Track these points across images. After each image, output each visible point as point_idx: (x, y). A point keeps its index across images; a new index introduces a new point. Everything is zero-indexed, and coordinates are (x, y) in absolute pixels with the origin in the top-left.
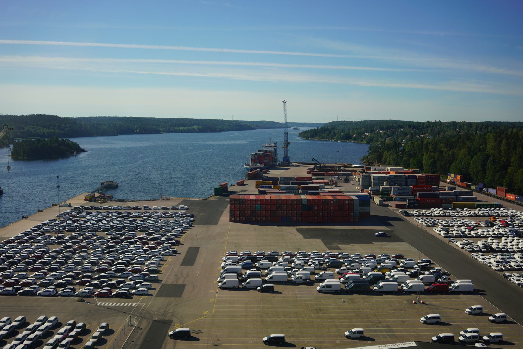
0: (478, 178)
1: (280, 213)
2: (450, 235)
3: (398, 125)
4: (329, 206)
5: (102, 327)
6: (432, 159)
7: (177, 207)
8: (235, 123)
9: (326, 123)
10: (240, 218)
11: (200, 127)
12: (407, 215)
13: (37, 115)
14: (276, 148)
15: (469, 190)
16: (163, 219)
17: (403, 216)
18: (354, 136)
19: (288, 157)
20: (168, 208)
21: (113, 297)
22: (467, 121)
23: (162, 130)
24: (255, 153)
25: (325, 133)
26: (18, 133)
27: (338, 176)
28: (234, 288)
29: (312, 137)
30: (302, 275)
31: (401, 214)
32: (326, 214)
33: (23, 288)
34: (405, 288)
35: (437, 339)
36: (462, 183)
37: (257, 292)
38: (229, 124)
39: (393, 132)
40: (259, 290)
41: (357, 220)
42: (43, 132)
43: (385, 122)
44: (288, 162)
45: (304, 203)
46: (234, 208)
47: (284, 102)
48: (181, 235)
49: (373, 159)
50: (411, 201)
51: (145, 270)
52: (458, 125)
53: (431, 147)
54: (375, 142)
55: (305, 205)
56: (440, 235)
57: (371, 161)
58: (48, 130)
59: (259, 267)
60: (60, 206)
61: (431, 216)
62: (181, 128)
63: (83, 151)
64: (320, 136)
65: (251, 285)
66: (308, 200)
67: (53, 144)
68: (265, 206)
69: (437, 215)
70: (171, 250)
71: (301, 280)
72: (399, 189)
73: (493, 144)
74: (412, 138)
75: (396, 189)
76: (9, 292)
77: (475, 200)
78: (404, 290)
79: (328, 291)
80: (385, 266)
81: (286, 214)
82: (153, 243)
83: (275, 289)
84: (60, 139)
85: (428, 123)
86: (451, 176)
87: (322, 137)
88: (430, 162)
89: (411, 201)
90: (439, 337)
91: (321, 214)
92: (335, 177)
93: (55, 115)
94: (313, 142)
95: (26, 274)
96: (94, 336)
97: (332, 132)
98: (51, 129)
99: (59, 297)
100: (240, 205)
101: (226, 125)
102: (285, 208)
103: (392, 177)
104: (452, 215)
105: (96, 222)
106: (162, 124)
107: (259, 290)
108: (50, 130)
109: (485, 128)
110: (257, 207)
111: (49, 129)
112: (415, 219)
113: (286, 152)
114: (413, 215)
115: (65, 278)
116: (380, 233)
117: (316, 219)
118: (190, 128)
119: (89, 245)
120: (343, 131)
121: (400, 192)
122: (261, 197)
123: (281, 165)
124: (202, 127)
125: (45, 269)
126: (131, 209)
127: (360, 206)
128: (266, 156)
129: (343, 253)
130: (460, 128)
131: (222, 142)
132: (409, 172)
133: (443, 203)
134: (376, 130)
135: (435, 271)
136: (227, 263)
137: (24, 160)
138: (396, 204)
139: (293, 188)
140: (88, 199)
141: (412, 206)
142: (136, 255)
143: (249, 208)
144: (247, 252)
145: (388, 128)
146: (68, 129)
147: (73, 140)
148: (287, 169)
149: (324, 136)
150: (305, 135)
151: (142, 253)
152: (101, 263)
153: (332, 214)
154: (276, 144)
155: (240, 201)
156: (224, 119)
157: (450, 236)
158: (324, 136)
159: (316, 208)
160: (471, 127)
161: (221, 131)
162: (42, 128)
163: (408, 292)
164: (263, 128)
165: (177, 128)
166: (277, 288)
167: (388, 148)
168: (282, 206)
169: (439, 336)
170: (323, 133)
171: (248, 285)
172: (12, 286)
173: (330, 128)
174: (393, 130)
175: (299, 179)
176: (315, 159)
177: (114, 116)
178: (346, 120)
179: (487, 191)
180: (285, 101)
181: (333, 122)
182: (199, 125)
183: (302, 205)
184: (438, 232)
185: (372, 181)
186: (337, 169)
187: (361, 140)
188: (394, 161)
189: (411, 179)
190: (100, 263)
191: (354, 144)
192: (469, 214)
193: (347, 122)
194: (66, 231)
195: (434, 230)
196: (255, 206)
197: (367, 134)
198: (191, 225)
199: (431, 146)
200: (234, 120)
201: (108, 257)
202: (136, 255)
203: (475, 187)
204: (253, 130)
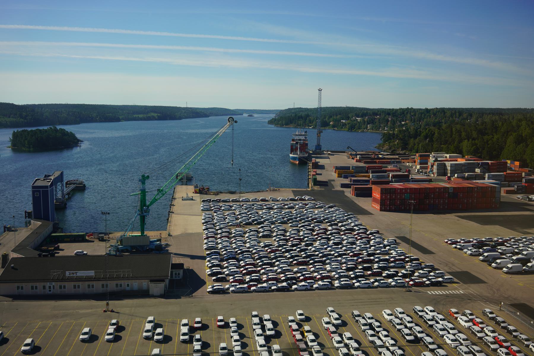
1: (427, 202)
3: (373, 112)
4: (473, 193)
5: (113, 324)
6: (475, 147)
9: (281, 110)
10: (390, 207)
11: (159, 114)
20: (267, 199)
21: (273, 291)
24: (379, 144)
29: (287, 124)
31: (521, 199)
32: (470, 201)
38: (184, 111)
42: (5, 121)
45: (450, 191)
46: (385, 198)
54: (357, 129)
55: (451, 193)
59: (503, 253)
60: (182, 200)
62: (141, 116)
64: (295, 124)
66: (454, 187)
68: (414, 195)
75: (490, 176)
76: (243, 289)
91: (465, 201)
94: (288, 129)
98: (12, 117)
100: (390, 194)
101: (182, 112)
102: (432, 196)
110: (407, 196)
111: (9, 117)
113: (319, 140)
119: (232, 240)
126: (258, 201)
130: (435, 115)
134: (352, 117)
137: (30, 152)
138: (507, 190)
141: (520, 191)
142: (223, 250)
143: (399, 197)
144: (254, 243)
147: (68, 128)
149: (300, 123)
150: (279, 123)
153: (475, 201)
156: (178, 106)
158: (300, 123)
159: (461, 195)
161: (180, 118)
163: (528, 272)
165: (137, 116)
170: (298, 120)
175: (370, 168)
176: (350, 147)
181: (289, 109)
182: (155, 112)
187: (340, 127)
193: (302, 108)
197: (344, 121)
202: (223, 250)
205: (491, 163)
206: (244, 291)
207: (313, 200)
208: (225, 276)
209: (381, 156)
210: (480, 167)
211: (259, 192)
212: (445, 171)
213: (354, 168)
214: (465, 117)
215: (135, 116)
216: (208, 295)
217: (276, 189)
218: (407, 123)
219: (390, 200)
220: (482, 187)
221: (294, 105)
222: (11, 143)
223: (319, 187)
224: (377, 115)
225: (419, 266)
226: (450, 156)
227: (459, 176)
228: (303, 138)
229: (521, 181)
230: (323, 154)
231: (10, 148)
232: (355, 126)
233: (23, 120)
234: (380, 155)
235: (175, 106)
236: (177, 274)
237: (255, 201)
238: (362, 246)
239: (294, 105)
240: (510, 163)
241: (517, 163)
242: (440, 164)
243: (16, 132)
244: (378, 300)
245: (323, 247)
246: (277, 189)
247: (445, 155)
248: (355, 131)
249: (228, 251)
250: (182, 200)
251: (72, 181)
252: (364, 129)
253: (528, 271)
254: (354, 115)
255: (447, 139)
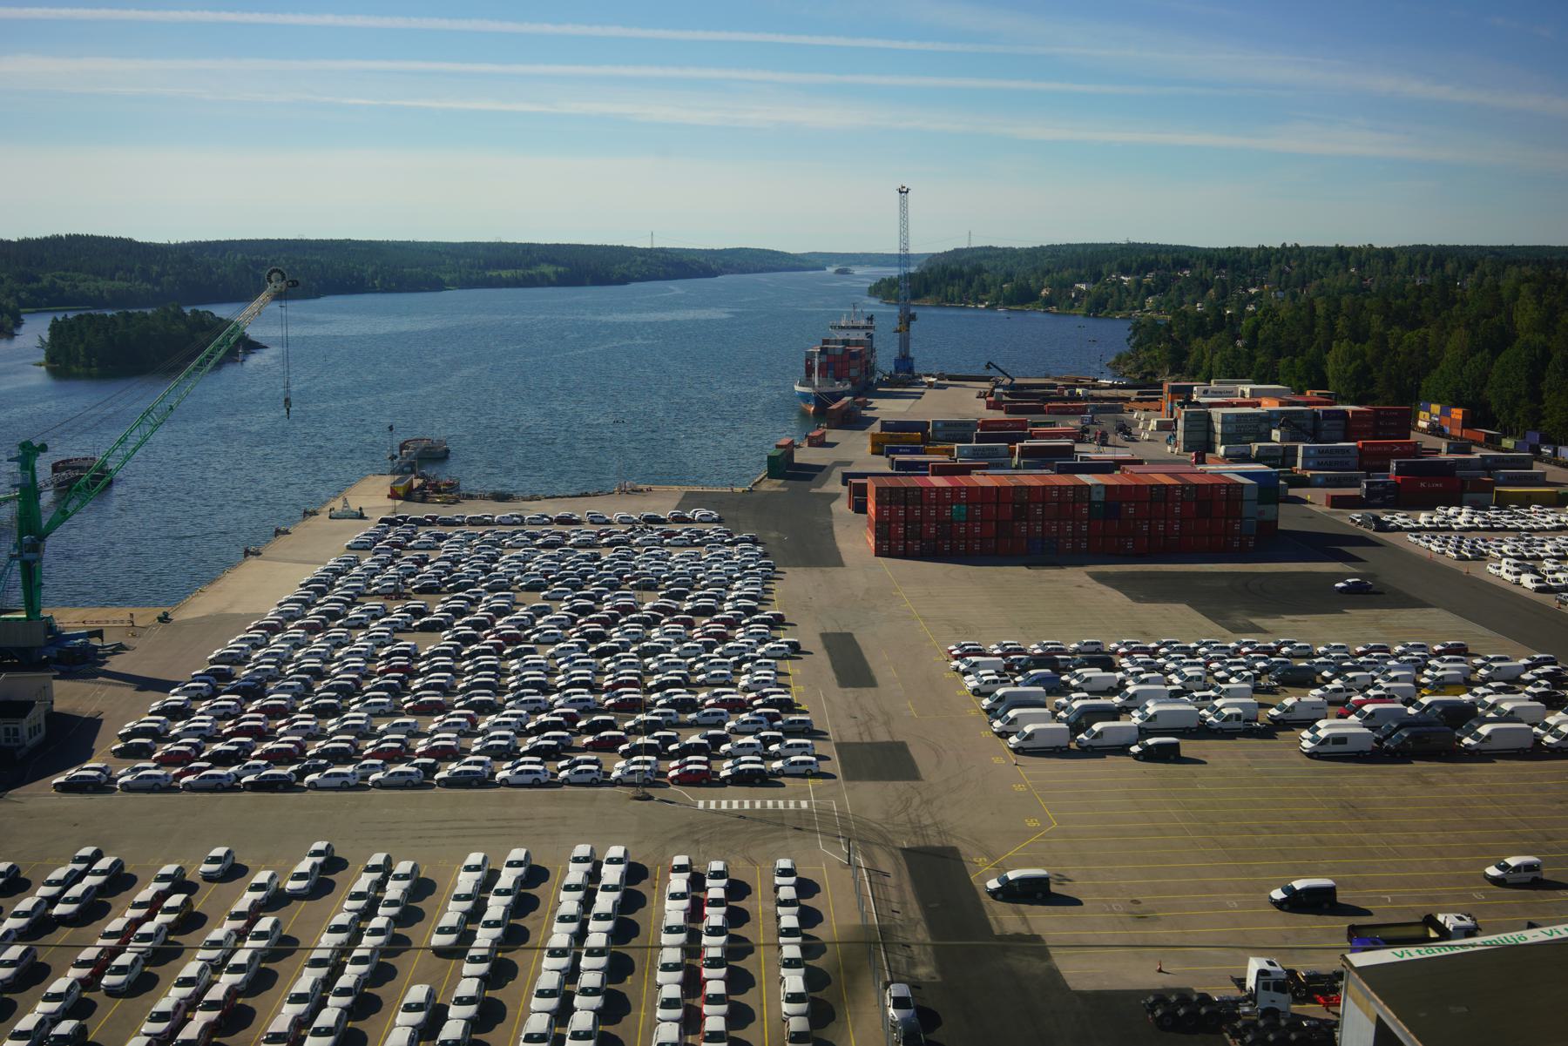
0: (1517, 415)
1: (1024, 529)
2: (1552, 584)
3: (1173, 259)
4: (1077, 505)
7: (689, 515)
8: (661, 255)
9: (934, 255)
10: (905, 545)
11: (560, 269)
12: (1382, 527)
13: (69, 237)
14: (871, 332)
15: (1498, 450)
16: (408, 555)
17: (1371, 532)
18: (1044, 292)
19: (912, 359)
21: (723, 782)
22: (1378, 245)
23: (447, 278)
25: (953, 285)
26: (23, 295)
27: (1091, 413)
28: (1058, 750)
30: (1238, 710)
31: (1359, 523)
32: (1161, 528)
33: (388, 766)
34: (1549, 739)
35: (1284, 896)
36: (1470, 431)
37: (1131, 760)
38: (643, 258)
39: (1162, 280)
40: (1136, 756)
41: (1251, 544)
42: (98, 288)
43: (1131, 248)
44: (910, 376)
45: (1095, 497)
46: (890, 517)
47: (901, 192)
48: (766, 596)
49: (1154, 362)
50: (1375, 488)
51: (457, 706)
52: (1351, 258)
53: (1342, 323)
54: (1112, 310)
55: (1099, 502)
56: (1518, 583)
57: (1148, 369)
58: (111, 283)
60: (330, 517)
61: (1450, 529)
62: (505, 274)
63: (252, 346)
65: (1107, 741)
66: (1107, 487)
67: (174, 327)
69: (1467, 525)
70: (700, 643)
71: (1239, 725)
72: (1320, 451)
73: (1536, 315)
74: (1223, 298)
76: (217, 781)
77: (1539, 480)
78: (1548, 744)
79: (1334, 752)
80: (1442, 677)
81: (1043, 529)
82: (378, 626)
83: (1184, 752)
84: (187, 310)
85: (1261, 252)
86: (1429, 411)
87: (947, 296)
88: (1351, 369)
89: (1375, 488)
90: (1290, 891)
91: (1145, 528)
92: (1082, 419)
93: (124, 236)
95: (416, 722)
96: (237, 913)
97: (976, 281)
98: (120, 279)
99: (567, 789)
100: (906, 504)
102: (1039, 511)
103: (1275, 415)
104: (1509, 526)
105: (414, 563)
106: (447, 261)
107: (1136, 756)
108: (117, 284)
109: (1434, 267)
110: (958, 511)
111: (112, 279)
112: (1413, 539)
113: (905, 344)
114: (1399, 529)
115: (232, 737)
116: (1350, 581)
117: (1130, 545)
118: (530, 272)
120: (1009, 277)
121: (1324, 460)
122: (905, 482)
123: (893, 381)
124: (568, 269)
125: (300, 709)
126: (552, 522)
127: (1259, 504)
128: (854, 356)
129: (1171, 643)
130: (1360, 266)
131: (652, 314)
132: (1313, 402)
133: (1468, 492)
134: (1109, 275)
135: (1381, 692)
136: (756, 678)
137: (89, 377)
138: (1333, 497)
139: (993, 453)
140: (401, 492)
141: (1378, 501)
142: (562, 659)
143: (933, 513)
145: (1145, 267)
146: (171, 278)
148: (918, 396)
151: (578, 651)
152: (369, 687)
153: (1177, 527)
154: (870, 319)
155: (906, 492)
157: (1551, 586)
159: (1131, 510)
160: (1394, 263)
161: (624, 280)
162: (91, 276)
164: (743, 271)
166: (1188, 748)
167: (1202, 328)
168: (1124, 505)
169: (1293, 888)
170: (948, 285)
171: (1097, 742)
172: (185, 762)
173: (966, 269)
174: (1161, 273)
176: (995, 363)
177: (554, 242)
178: (994, 245)
179: (1555, 453)
180: (905, 190)
181: (957, 250)
182: (553, 262)
183: (1091, 503)
184: (1510, 577)
185: (1218, 427)
186: (1066, 393)
187: (1066, 303)
188: (1228, 366)
189: (1330, 422)
190: (413, 688)
191: (1045, 316)
192: (1558, 521)
193: (996, 249)
194: (414, 590)
195: (1493, 571)
196: (951, 509)
197: (1083, 287)
198: (773, 568)
199: (1344, 320)
200: (657, 245)
201: (292, 671)
202: (562, 659)
203: (1513, 443)
204: (715, 276)
205: (1353, 412)
206: (157, 787)
207: (714, 521)
208: (623, 734)
209: (1080, 391)
210: (1282, 425)
211: (586, 495)
212: (1208, 436)
213: (939, 425)
214: (1450, 273)
215: (488, 274)
216: (53, 795)
217: (640, 487)
218: (1266, 294)
219: (906, 523)
220: (1197, 485)
221: (652, 241)
222: (44, 352)
223: (781, 481)
224: (1184, 265)
225: (761, 722)
226: (1252, 390)
227: (1231, 452)
228: (861, 335)
229: (1387, 469)
230: (916, 384)
231: (43, 368)
232: (1107, 300)
233: (149, 286)
234: (1080, 387)
235: (620, 244)
236: (11, 732)
237: (538, 521)
238: (1184, 661)
239: (652, 241)
240: (1438, 412)
241: (1457, 414)
242: (1193, 414)
243: (60, 319)
244: (515, 824)
245: (683, 661)
246: (645, 487)
247: (1241, 388)
248: (1106, 316)
249: (622, 661)
250: (330, 517)
251: (76, 459)
252: (1134, 308)
253: (1090, 746)
254: (1115, 267)
255: (1294, 339)
